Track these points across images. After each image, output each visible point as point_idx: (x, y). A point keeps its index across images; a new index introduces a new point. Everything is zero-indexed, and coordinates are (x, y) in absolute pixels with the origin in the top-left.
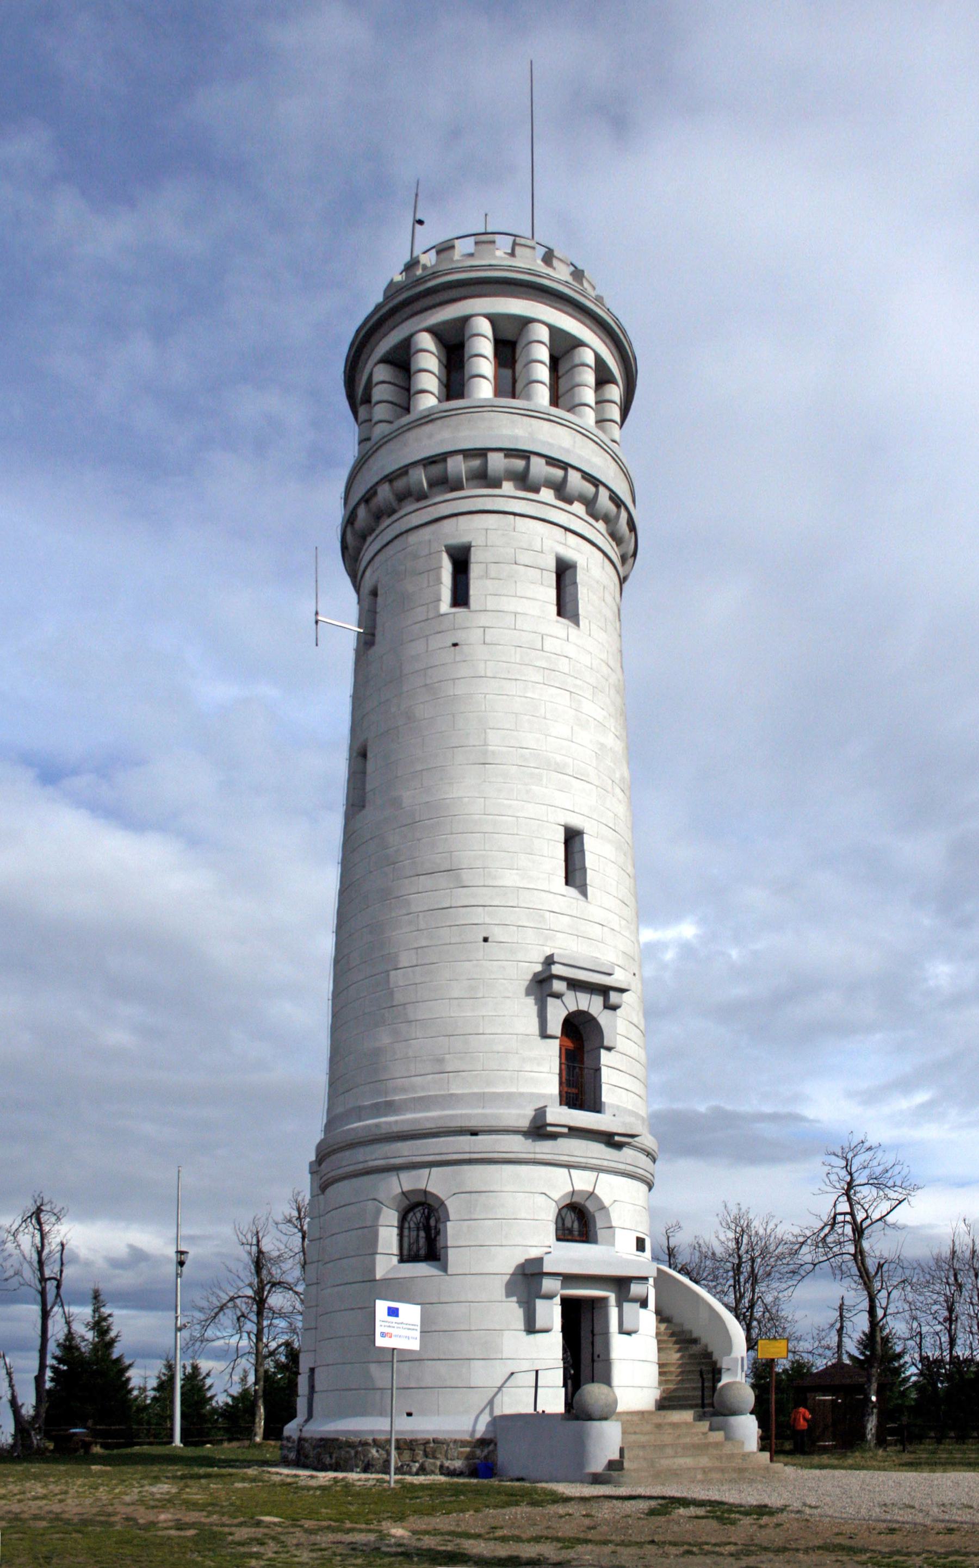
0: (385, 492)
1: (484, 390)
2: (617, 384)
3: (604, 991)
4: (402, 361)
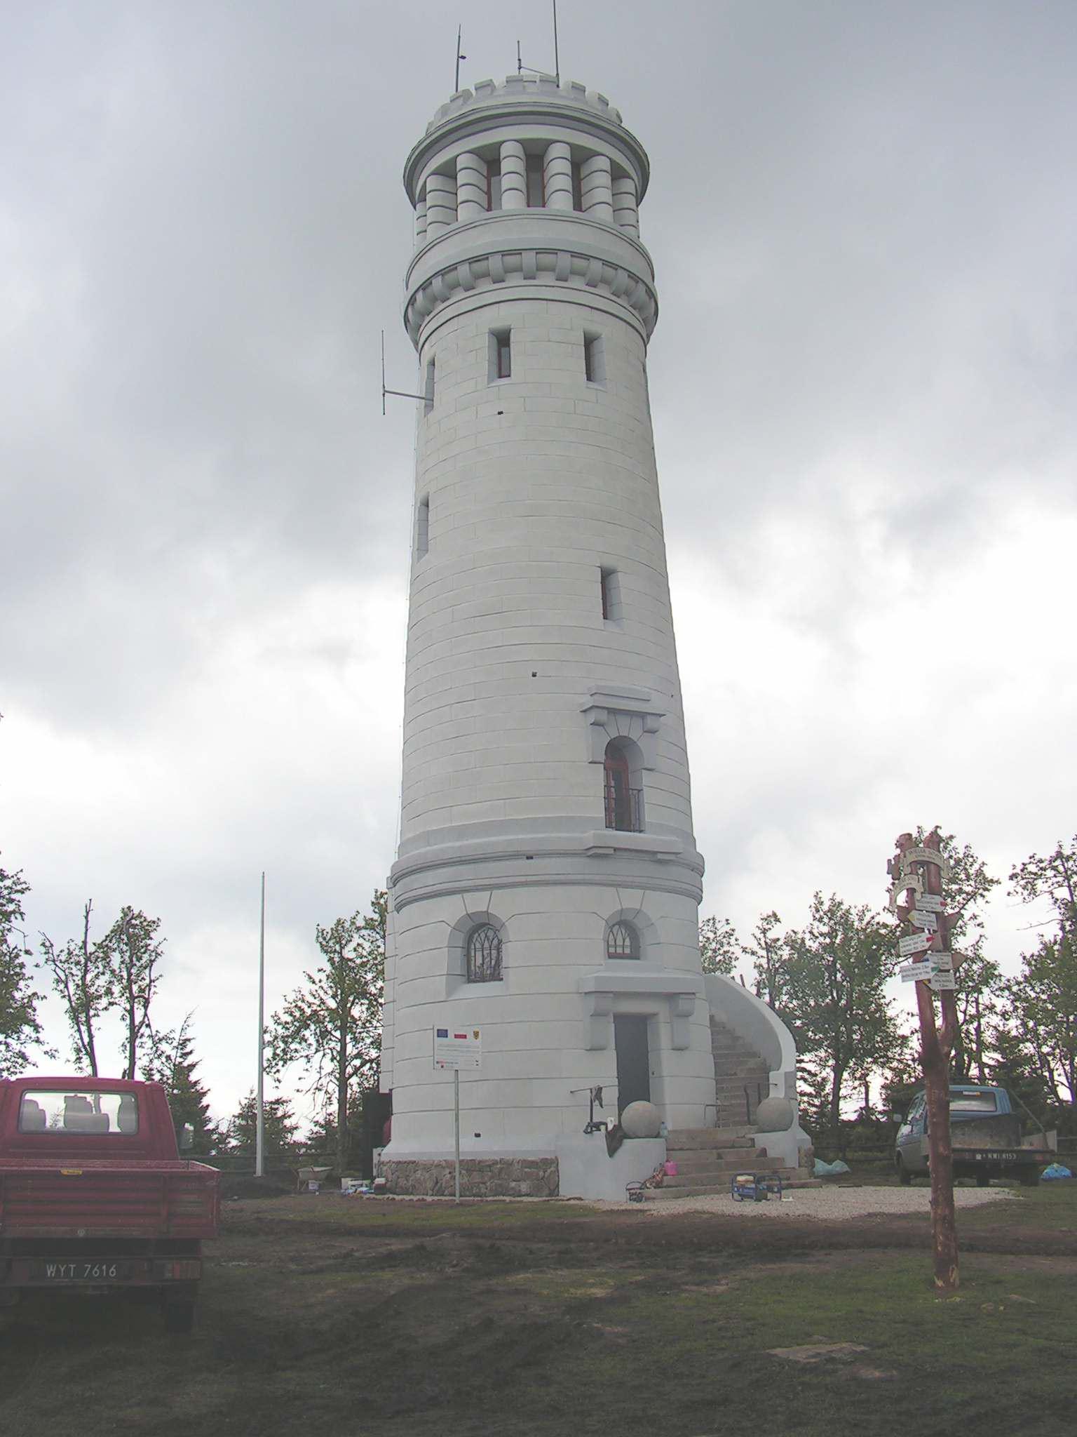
0: (437, 283)
1: (512, 201)
2: (629, 177)
3: (642, 715)
4: (448, 172)
